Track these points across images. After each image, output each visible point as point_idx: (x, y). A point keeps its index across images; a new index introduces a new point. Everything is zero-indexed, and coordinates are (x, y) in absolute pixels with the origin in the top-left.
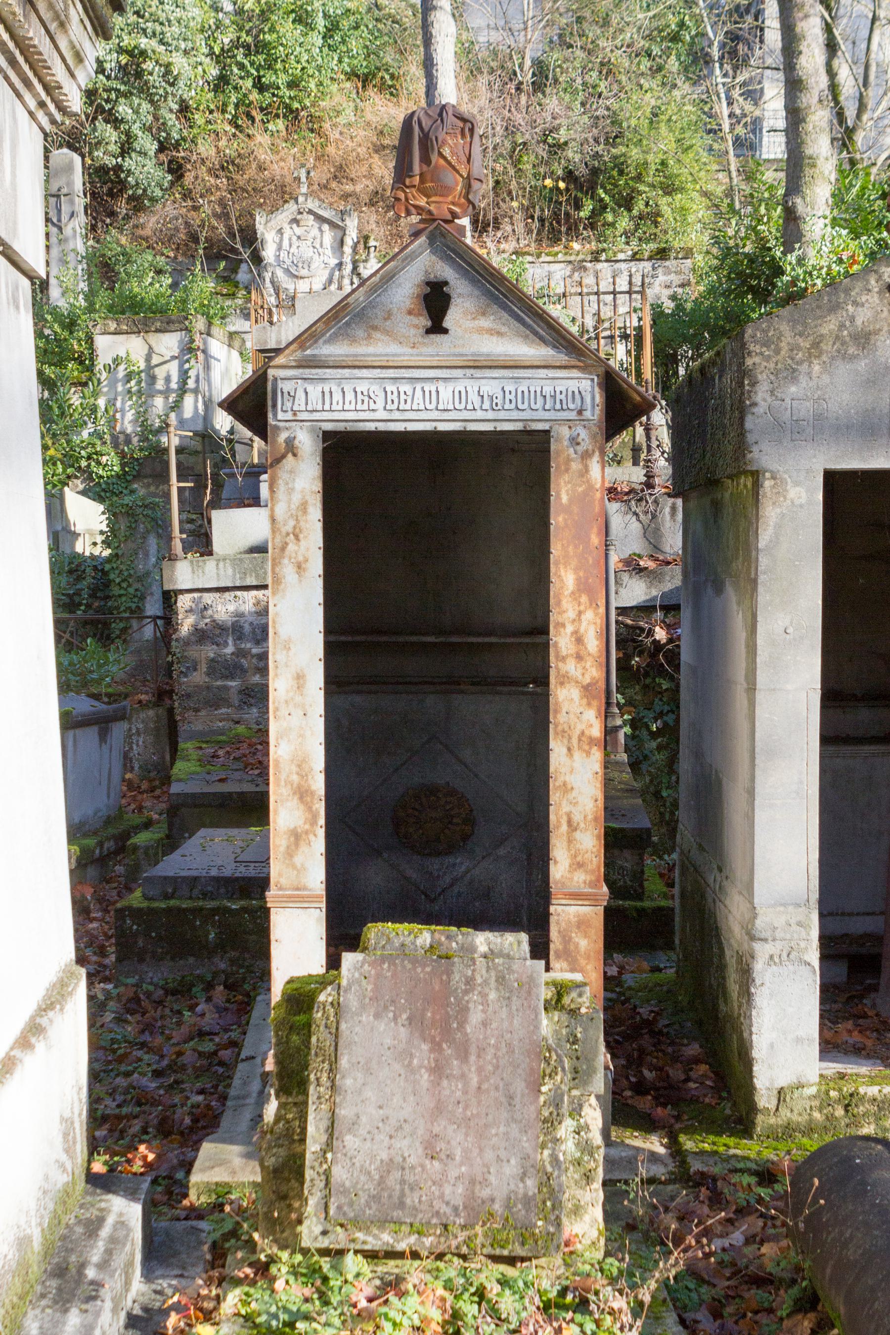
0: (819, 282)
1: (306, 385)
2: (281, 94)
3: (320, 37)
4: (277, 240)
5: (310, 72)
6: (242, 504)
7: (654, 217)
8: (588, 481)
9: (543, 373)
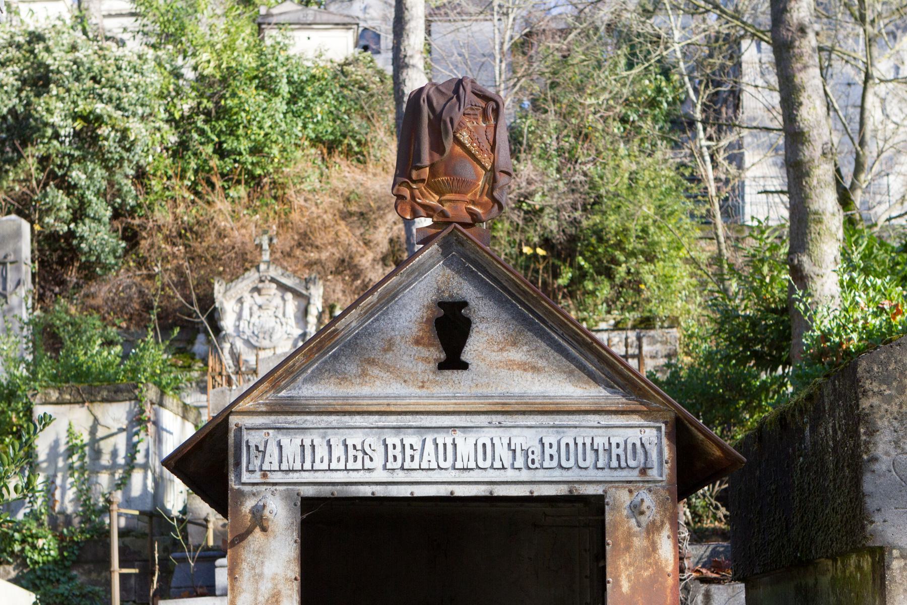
0: (855, 336)
1: (280, 437)
2: (243, 159)
3: (284, 102)
4: (237, 309)
5: (274, 138)
6: (194, 593)
7: (635, 283)
8: (656, 563)
9: (593, 419)
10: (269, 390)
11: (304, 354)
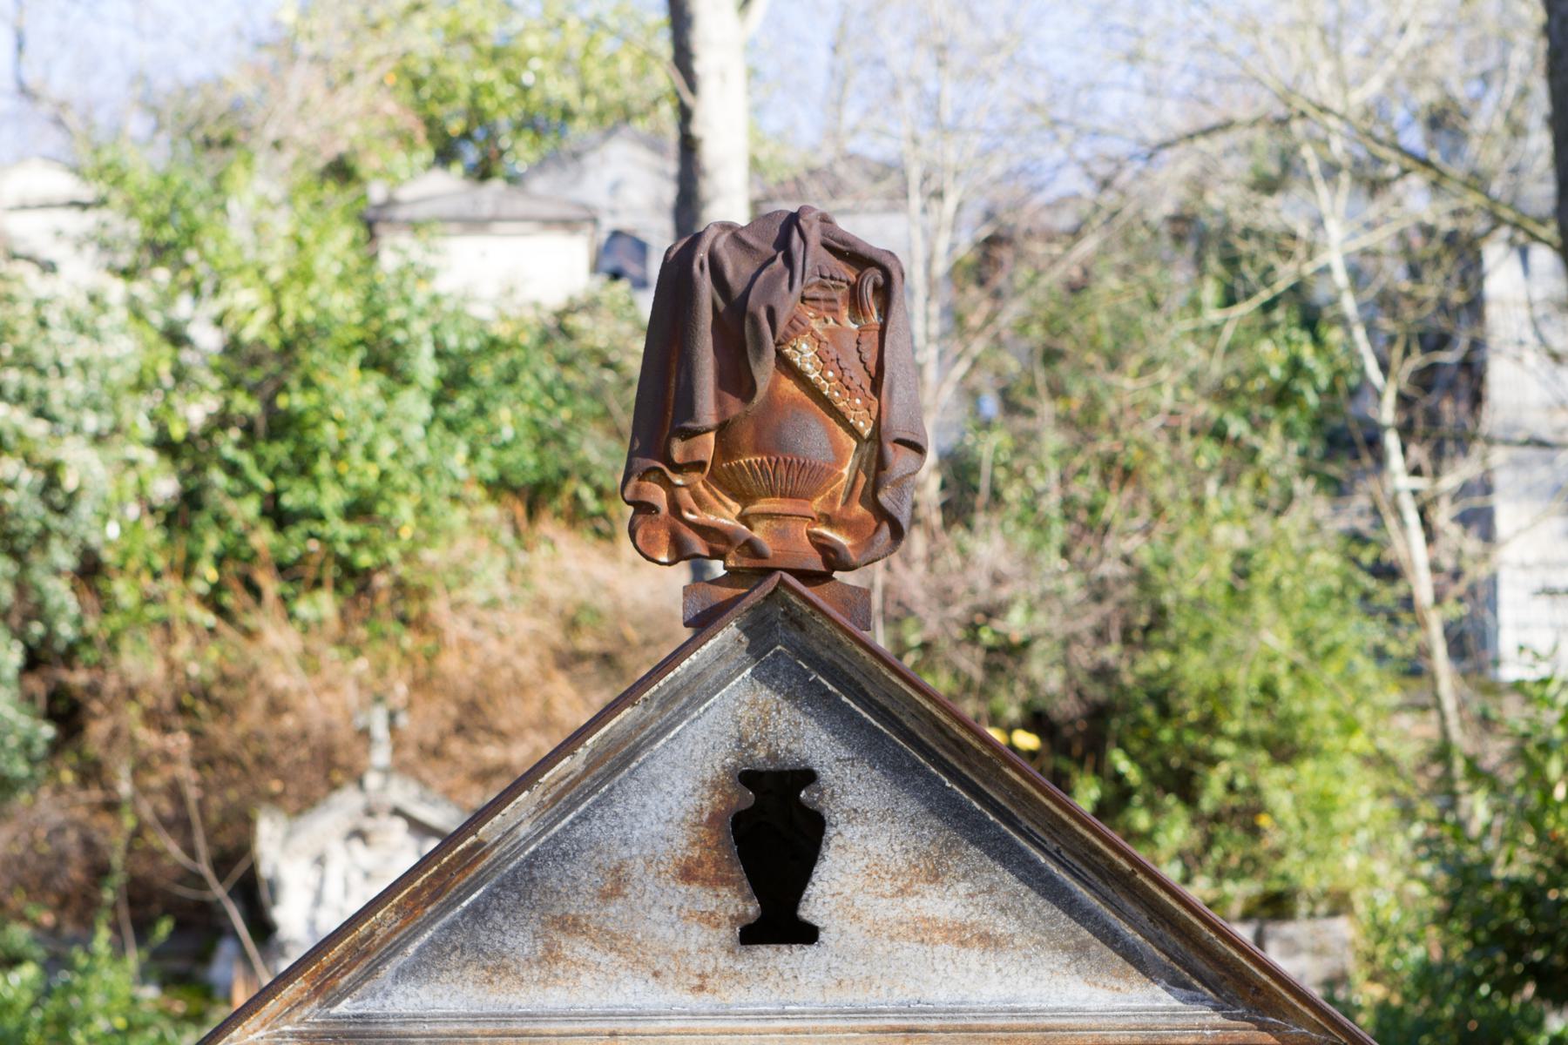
7: (1246, 814)
10: (309, 1000)
11: (399, 907)
